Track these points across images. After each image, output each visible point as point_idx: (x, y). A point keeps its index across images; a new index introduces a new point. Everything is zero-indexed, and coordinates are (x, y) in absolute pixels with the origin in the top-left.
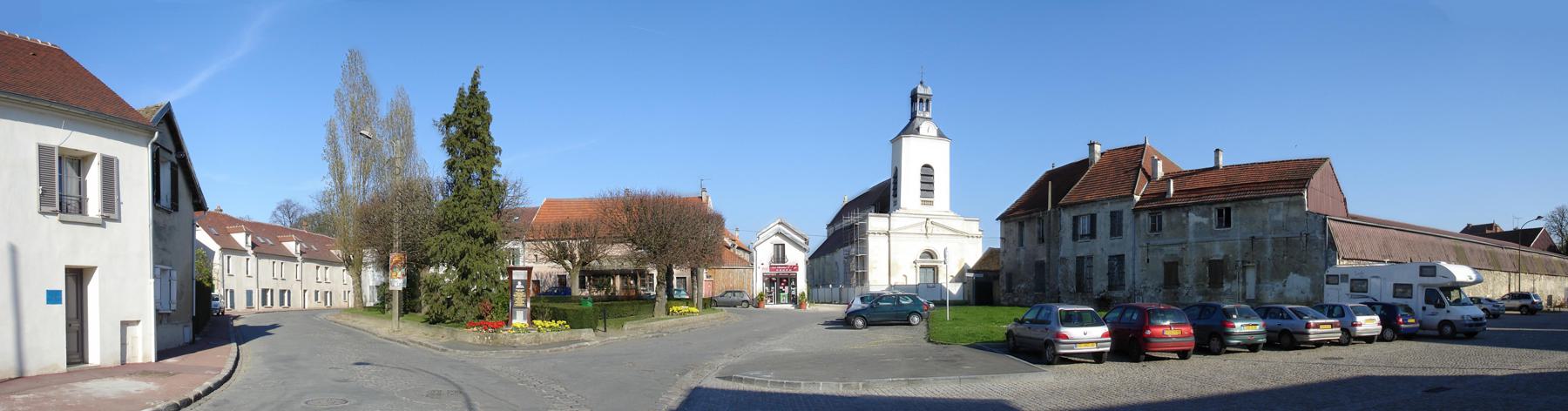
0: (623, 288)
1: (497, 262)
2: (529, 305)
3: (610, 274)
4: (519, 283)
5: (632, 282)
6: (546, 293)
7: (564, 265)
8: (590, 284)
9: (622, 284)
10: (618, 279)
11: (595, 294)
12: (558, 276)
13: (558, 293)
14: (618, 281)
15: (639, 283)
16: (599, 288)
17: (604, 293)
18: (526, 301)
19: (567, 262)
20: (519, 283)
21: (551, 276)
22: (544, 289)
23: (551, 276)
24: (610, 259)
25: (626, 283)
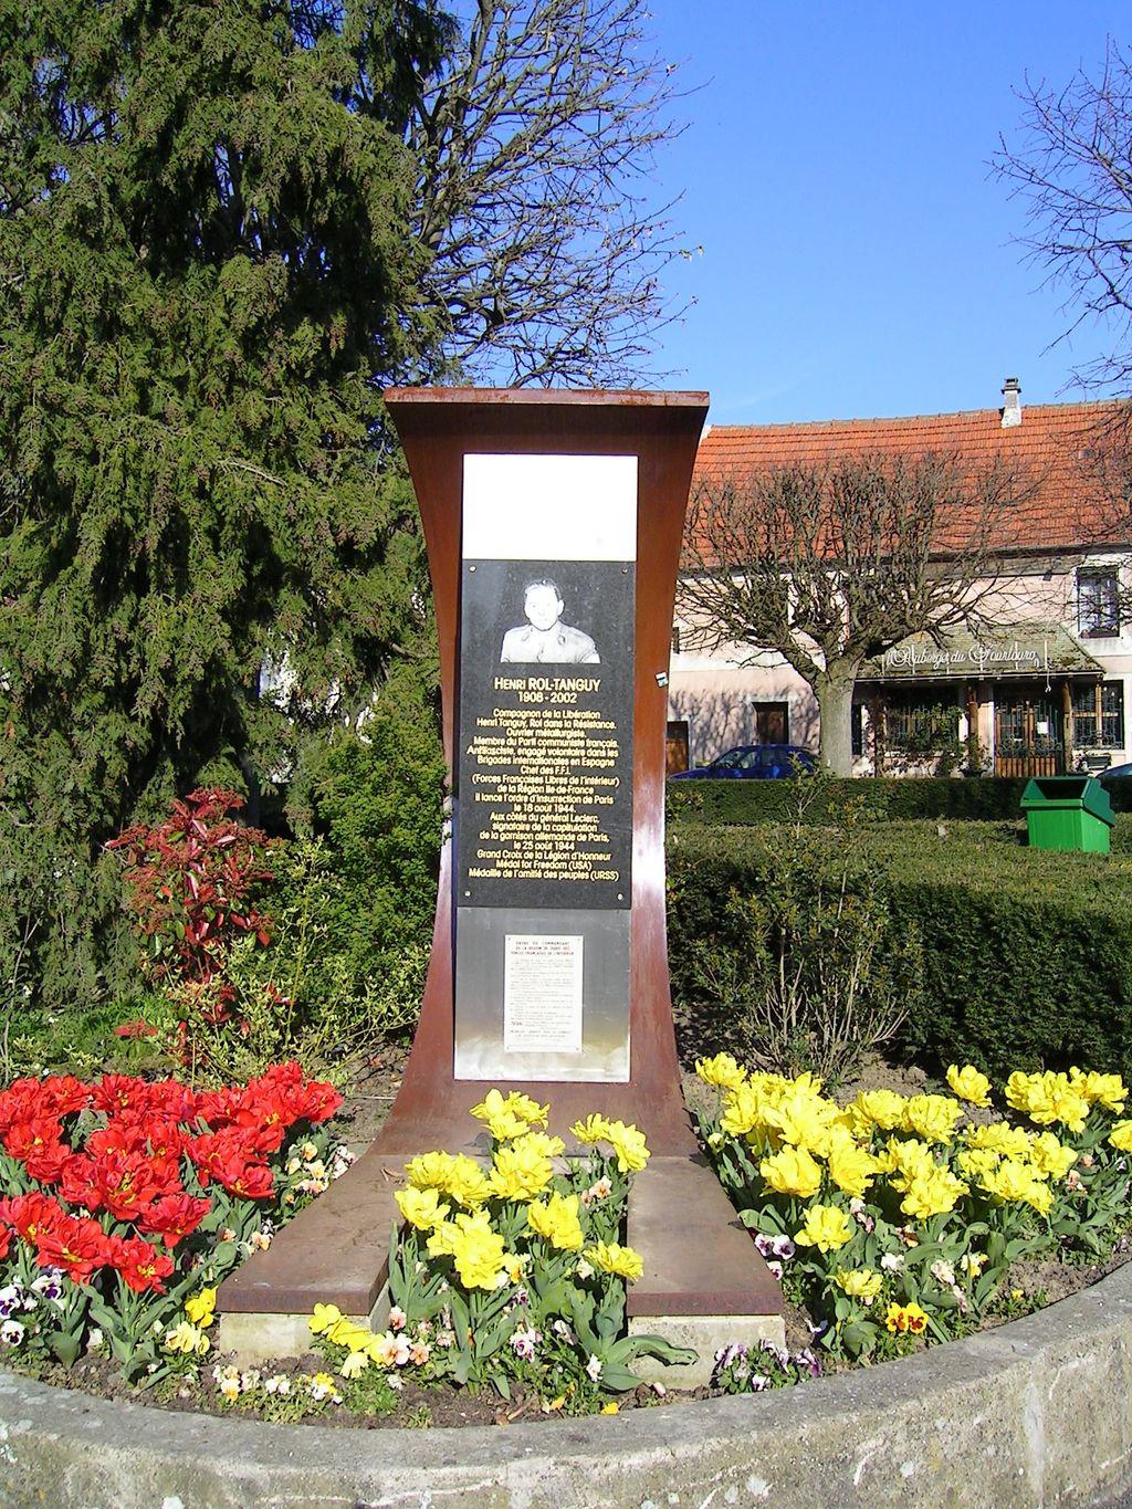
0: (1003, 751)
1: (221, 891)
2: (649, 870)
3: (955, 693)
4: (542, 601)
5: (1043, 728)
6: (714, 770)
7: (791, 653)
8: (879, 737)
9: (1001, 735)
10: (987, 714)
11: (896, 774)
12: (757, 705)
13: (759, 771)
14: (987, 714)
15: (1070, 733)
16: (915, 749)
17: (932, 770)
18: (617, 824)
19: (802, 638)
20: (542, 601)
21: (727, 709)
22: (705, 756)
23: (727, 709)
24: (985, 630)
25: (1020, 732)
